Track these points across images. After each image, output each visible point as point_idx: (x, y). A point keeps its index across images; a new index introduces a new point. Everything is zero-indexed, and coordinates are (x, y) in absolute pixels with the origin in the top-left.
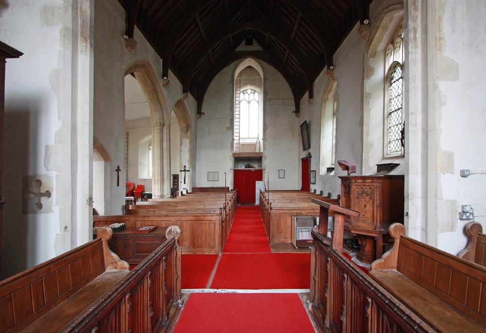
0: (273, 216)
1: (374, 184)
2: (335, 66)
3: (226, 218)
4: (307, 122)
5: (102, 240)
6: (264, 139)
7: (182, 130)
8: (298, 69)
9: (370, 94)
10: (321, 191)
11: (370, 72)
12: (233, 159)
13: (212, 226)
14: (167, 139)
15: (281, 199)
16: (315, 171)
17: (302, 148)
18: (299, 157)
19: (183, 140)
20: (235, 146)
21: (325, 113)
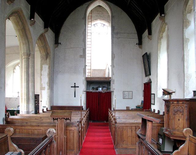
0: (118, 128)
1: (184, 105)
2: (166, 14)
3: (81, 129)
4: (148, 53)
5: (8, 136)
6: (113, 66)
7: (42, 57)
8: (139, 10)
9: (188, 39)
10: (158, 111)
11: (188, 24)
12: (85, 82)
13: (72, 134)
14: (32, 66)
15: (126, 116)
16: (154, 94)
17: (144, 75)
18: (142, 83)
19: (43, 66)
20: (87, 71)
21: (160, 48)
